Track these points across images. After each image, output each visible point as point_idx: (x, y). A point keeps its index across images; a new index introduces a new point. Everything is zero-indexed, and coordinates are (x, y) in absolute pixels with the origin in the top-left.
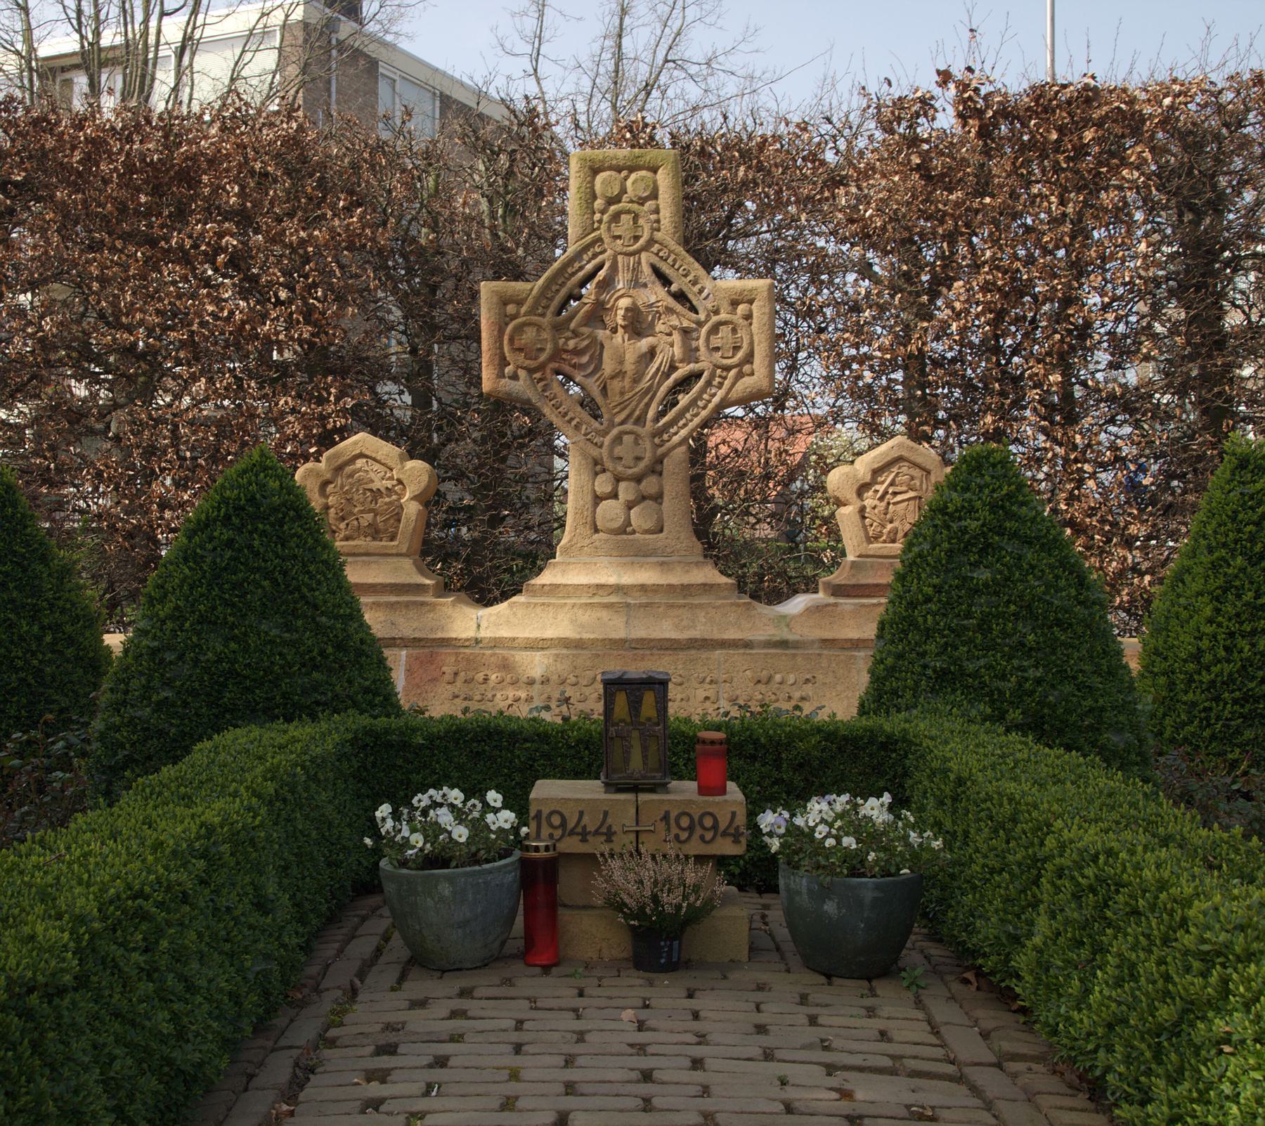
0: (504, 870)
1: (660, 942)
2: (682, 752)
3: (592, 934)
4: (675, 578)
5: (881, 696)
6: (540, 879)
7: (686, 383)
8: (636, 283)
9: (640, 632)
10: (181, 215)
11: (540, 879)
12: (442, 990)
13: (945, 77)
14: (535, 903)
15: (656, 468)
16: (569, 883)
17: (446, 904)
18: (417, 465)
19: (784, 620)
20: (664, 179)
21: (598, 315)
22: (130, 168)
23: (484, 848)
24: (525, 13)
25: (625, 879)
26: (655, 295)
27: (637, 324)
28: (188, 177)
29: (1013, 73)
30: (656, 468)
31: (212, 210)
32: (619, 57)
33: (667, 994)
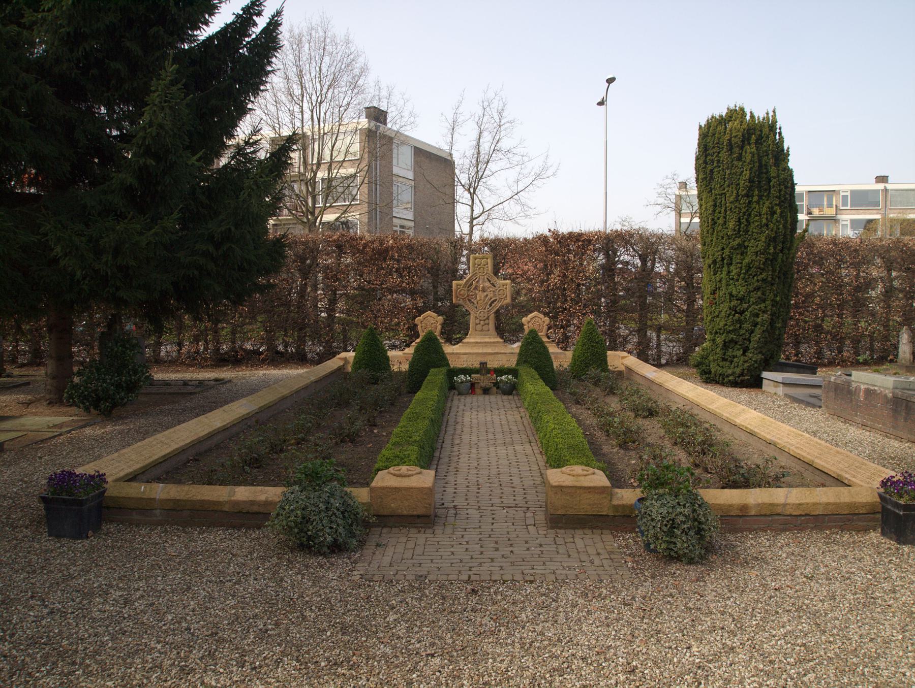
0: (469, 384)
1: (486, 391)
2: (489, 371)
3: (478, 391)
4: (492, 340)
5: (517, 364)
6: (473, 385)
7: (493, 302)
8: (484, 281)
9: (485, 351)
10: (385, 260)
11: (473, 385)
12: (463, 397)
13: (550, 231)
14: (472, 388)
15: (488, 318)
16: (476, 386)
17: (463, 388)
18: (440, 317)
19: (513, 349)
20: (489, 261)
21: (476, 288)
22: (373, 250)
23: (467, 381)
24: (446, 136)
25: (483, 385)
26: (487, 284)
27: (484, 290)
28: (386, 250)
29: (564, 229)
30: (488, 318)
31: (392, 258)
32: (478, 153)
33: (487, 397)
